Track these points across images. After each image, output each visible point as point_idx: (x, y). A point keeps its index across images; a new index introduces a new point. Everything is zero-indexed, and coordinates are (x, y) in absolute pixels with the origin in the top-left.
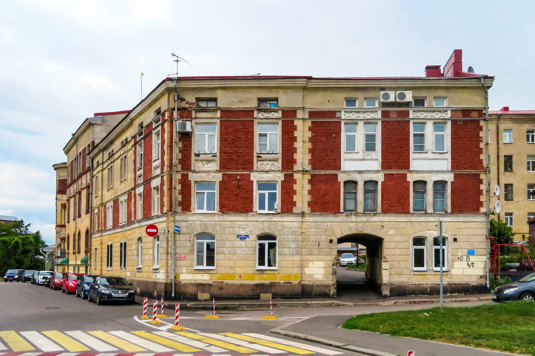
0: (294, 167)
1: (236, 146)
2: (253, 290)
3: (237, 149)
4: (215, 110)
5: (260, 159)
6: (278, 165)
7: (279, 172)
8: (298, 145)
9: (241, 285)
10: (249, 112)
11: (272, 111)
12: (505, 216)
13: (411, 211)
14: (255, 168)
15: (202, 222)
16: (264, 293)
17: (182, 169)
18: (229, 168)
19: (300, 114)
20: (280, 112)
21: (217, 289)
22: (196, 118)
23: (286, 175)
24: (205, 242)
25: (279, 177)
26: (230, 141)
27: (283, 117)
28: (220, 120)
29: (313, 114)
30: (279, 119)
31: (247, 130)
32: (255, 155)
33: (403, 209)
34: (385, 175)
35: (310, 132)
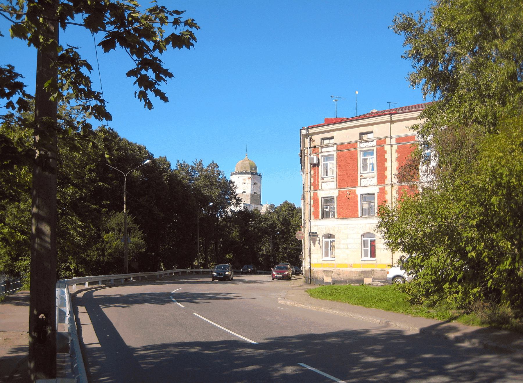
0: (386, 182)
1: (347, 170)
2: (359, 275)
3: (347, 172)
4: (333, 145)
5: (363, 177)
6: (375, 180)
7: (375, 186)
8: (388, 164)
9: (351, 271)
10: (353, 145)
11: (363, 142)
12: (356, 217)
13: (359, 216)
14: (359, 185)
15: (372, 225)
16: (367, 277)
17: (313, 189)
18: (342, 186)
19: (388, 141)
20: (375, 141)
21: (337, 274)
22: (321, 152)
23: (380, 189)
24: (369, 239)
25: (375, 190)
26: (343, 166)
27: (377, 144)
28: (336, 152)
29: (399, 140)
30: (374, 147)
31: (353, 157)
32: (359, 175)
33: (353, 215)
34: (339, 191)
35: (397, 154)
